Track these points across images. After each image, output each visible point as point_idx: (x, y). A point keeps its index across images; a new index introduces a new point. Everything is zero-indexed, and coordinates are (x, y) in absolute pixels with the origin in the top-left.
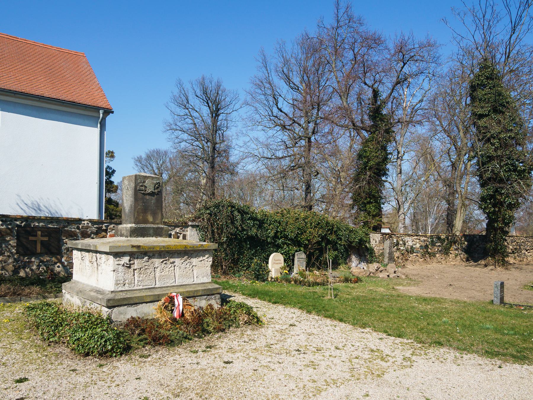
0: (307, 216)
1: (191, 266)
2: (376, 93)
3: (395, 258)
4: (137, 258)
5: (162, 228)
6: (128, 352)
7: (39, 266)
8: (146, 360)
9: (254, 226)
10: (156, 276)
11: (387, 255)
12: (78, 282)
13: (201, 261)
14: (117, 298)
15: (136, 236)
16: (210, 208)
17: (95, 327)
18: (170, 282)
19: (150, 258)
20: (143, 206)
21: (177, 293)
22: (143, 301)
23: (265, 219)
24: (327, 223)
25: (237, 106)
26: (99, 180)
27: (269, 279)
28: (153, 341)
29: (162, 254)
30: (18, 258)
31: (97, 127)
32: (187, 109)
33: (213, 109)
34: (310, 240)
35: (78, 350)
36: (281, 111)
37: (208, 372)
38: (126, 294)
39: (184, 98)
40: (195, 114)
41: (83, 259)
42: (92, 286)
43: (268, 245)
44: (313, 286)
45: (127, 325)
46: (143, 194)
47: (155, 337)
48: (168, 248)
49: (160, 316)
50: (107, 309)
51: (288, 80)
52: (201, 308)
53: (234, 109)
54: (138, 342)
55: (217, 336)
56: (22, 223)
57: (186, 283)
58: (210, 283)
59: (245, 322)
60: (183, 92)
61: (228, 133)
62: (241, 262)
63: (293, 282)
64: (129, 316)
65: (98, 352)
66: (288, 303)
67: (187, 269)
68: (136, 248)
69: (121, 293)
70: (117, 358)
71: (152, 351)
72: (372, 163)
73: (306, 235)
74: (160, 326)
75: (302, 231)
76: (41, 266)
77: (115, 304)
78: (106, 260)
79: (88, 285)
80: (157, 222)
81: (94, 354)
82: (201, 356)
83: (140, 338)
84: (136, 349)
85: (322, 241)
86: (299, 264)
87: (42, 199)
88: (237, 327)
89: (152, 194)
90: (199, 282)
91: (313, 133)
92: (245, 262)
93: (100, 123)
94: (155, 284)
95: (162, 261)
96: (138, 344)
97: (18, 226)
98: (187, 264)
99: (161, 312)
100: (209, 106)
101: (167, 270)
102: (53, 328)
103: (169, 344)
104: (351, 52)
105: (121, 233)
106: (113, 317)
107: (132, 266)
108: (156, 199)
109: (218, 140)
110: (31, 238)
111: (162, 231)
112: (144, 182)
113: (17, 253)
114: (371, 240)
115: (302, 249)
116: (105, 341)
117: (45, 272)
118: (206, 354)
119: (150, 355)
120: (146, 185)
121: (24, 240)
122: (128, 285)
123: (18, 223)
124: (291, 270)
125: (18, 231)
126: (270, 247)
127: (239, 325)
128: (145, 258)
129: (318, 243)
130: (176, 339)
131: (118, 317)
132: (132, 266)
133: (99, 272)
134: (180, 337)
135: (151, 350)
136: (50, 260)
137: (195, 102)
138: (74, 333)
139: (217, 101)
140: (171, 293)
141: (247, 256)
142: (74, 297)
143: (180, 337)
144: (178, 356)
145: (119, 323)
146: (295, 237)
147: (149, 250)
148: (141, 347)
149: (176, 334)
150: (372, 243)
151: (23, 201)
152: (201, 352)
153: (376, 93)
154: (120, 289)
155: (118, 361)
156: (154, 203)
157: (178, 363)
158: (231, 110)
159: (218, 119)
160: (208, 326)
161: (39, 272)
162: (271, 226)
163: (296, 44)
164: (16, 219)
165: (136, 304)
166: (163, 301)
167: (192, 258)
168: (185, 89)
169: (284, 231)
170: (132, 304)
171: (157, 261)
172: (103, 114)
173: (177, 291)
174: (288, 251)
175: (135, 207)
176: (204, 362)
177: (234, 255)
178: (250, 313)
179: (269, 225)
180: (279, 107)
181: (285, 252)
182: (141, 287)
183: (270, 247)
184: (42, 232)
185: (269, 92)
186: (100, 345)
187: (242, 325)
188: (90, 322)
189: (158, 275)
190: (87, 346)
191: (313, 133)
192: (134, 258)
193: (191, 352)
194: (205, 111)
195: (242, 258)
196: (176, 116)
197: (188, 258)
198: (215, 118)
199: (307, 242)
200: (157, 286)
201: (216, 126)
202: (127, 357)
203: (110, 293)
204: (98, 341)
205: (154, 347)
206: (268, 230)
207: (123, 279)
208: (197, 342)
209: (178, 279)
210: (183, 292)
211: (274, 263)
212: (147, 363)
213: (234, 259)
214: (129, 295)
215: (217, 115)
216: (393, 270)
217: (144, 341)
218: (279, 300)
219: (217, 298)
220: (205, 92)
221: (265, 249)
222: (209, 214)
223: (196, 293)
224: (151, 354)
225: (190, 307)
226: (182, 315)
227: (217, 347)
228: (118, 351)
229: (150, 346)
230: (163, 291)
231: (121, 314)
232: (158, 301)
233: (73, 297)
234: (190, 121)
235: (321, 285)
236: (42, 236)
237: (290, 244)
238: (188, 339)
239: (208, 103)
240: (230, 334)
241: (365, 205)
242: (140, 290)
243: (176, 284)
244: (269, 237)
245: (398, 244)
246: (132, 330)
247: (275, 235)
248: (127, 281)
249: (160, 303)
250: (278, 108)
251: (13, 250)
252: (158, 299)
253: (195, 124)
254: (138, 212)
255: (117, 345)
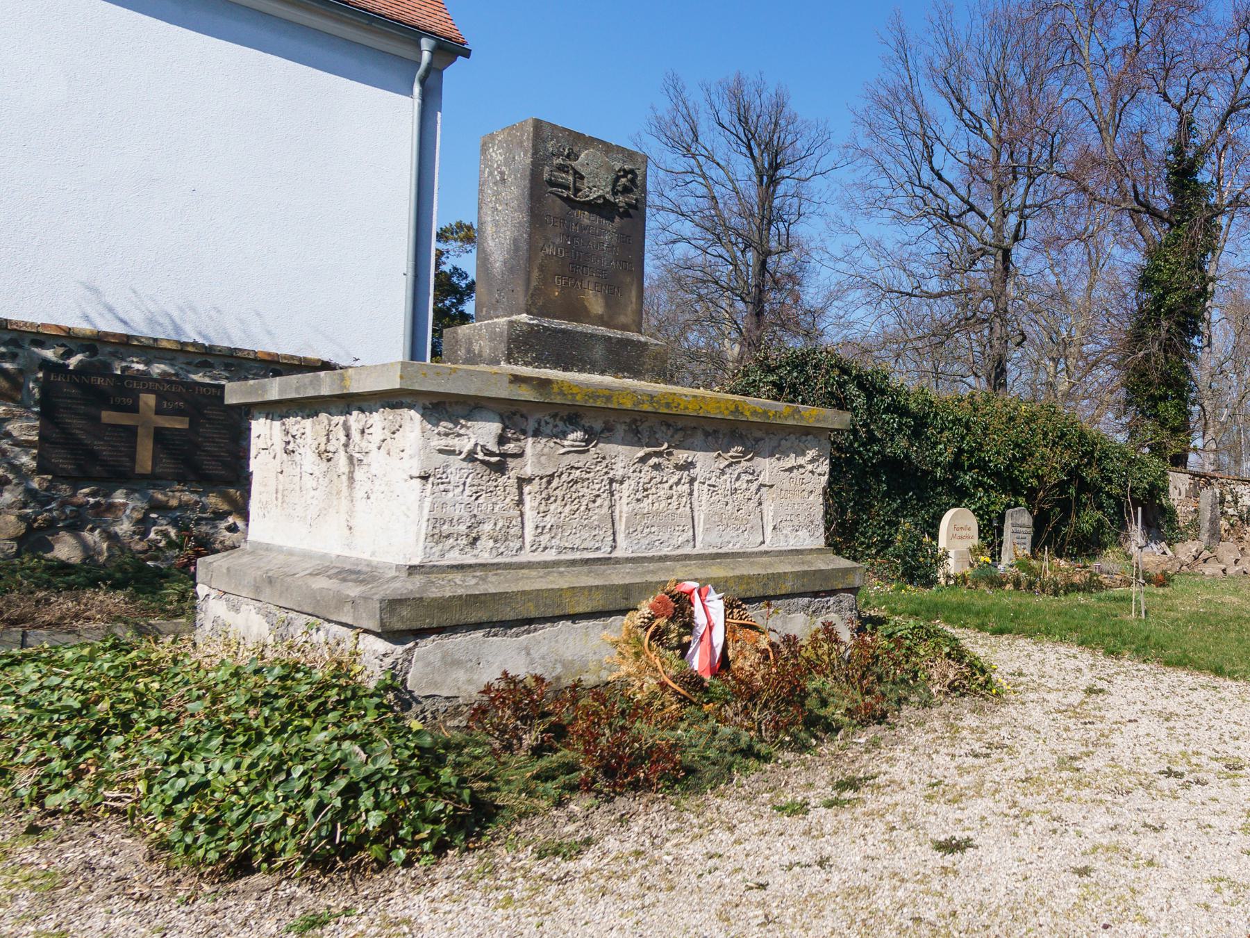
0: (1034, 414)
1: (754, 486)
2: (1186, 125)
3: (1223, 532)
4: (537, 434)
5: (644, 345)
6: (480, 836)
7: (143, 525)
8: (571, 865)
9: (899, 430)
10: (617, 513)
11: (1207, 525)
12: (268, 548)
13: (790, 470)
14: (434, 593)
15: (535, 360)
16: (778, 367)
17: (307, 722)
18: (672, 542)
19: (592, 437)
20: (568, 249)
21: (704, 582)
22: (558, 612)
23: (928, 414)
24: (1082, 436)
25: (825, 164)
26: (411, 264)
27: (942, 581)
28: (605, 774)
29: (644, 427)
30: (47, 489)
31: (410, 93)
32: (694, 156)
33: (763, 165)
34: (1043, 476)
35: (188, 847)
36: (940, 178)
37: (883, 901)
38: (484, 579)
39: (684, 127)
40: (715, 173)
41: (290, 447)
42: (324, 556)
43: (936, 487)
44: (1066, 594)
45: (480, 713)
46: (567, 200)
47: (614, 755)
48: (668, 405)
49: (633, 670)
50: (381, 646)
51: (958, 99)
52: (790, 641)
53: (818, 171)
54: (533, 785)
55: (863, 740)
56: (69, 354)
57: (736, 549)
58: (819, 551)
59: (949, 686)
60: (685, 112)
61: (801, 230)
62: (861, 533)
63: (1009, 587)
64: (491, 675)
65: (306, 850)
66: (1039, 630)
67: (739, 496)
68: (534, 388)
69: (458, 577)
70: (418, 869)
71: (601, 819)
72: (1172, 299)
73: (1035, 464)
74: (636, 711)
75: (1024, 451)
76: (155, 523)
77: (426, 623)
78: (388, 434)
79: (306, 555)
80: (622, 319)
81: (280, 863)
82: (828, 828)
83: (543, 763)
84: (523, 815)
85: (1069, 482)
86: (1016, 541)
87: (193, 309)
88: (926, 705)
89: (603, 208)
90: (783, 546)
91: (1016, 238)
92: (874, 533)
93: (423, 82)
94: (614, 548)
95: (641, 454)
96: (531, 793)
97: (45, 364)
98: (738, 479)
99: (637, 655)
100: (752, 154)
101: (661, 493)
102: (68, 742)
103: (677, 781)
104: (1130, 21)
105: (469, 351)
106: (415, 681)
107: (511, 463)
108: (620, 231)
109: (773, 244)
110: (107, 416)
111: (639, 356)
112: (572, 156)
113: (40, 470)
114: (1171, 489)
115: (1022, 500)
116: (352, 791)
117: (171, 544)
118: (845, 816)
119: (588, 842)
120: (579, 168)
121: (76, 425)
122: (491, 543)
123: (49, 354)
124: (996, 556)
125: (45, 387)
126: (940, 494)
127: (931, 696)
128: (571, 436)
129: (1062, 486)
130: (708, 758)
131: (438, 678)
132: (511, 463)
133: (359, 493)
134: (722, 750)
135: (596, 816)
136: (197, 503)
137: (715, 140)
138: (180, 760)
139: (775, 143)
140: (678, 581)
141: (878, 515)
142: (244, 607)
143: (722, 750)
144: (725, 836)
145: (442, 705)
146: (1007, 468)
147: (591, 403)
148: (544, 804)
149: (703, 741)
150: (1171, 497)
151: (111, 310)
152: (823, 811)
153: (1186, 125)
154: (454, 557)
155: (418, 885)
156: (610, 246)
157: (730, 868)
158: (810, 173)
159: (774, 191)
160: (824, 703)
161: (140, 546)
162: (946, 433)
163: (978, 16)
164: (40, 337)
165: (529, 621)
166: (645, 609)
167: (757, 454)
168: (690, 104)
169: (980, 450)
170: (507, 625)
171: (622, 456)
172: (433, 52)
173: (700, 574)
174: (988, 506)
175: (533, 247)
176: (849, 856)
177: (844, 512)
178: (963, 657)
179: (940, 433)
180: (936, 167)
181: (980, 508)
182: (551, 556)
183: (940, 494)
184: (160, 397)
185: (914, 126)
186: (316, 813)
187: (942, 697)
188: (282, 702)
189: (625, 509)
190: (239, 822)
191: (1016, 238)
192: (524, 432)
193: (780, 809)
194: (743, 168)
195: (867, 521)
196: (661, 173)
197: (745, 453)
198: (768, 187)
199: (1035, 482)
200: (618, 554)
201: (770, 207)
202: (470, 860)
203: (404, 574)
204: (307, 792)
205: (610, 800)
206: (935, 444)
207: (466, 515)
208: (792, 769)
209: (707, 530)
210: (727, 580)
211: (954, 536)
212: (578, 886)
213: (844, 522)
214: (493, 585)
215: (774, 182)
216: (1232, 557)
217: (562, 779)
218: (1010, 625)
219: (845, 604)
220: (743, 120)
221: (928, 499)
222: (774, 383)
223: (772, 584)
224: (595, 834)
225: (753, 633)
226: (723, 664)
227: (881, 780)
228: (424, 835)
229: (588, 800)
230: (644, 573)
231: (457, 663)
232: (623, 612)
233: (237, 611)
234: (701, 190)
235: (1084, 590)
236: (159, 411)
237: (992, 487)
238: (758, 756)
239: (749, 148)
240: (910, 729)
241: (1155, 400)
242: (545, 565)
243: (695, 551)
244: (938, 464)
245: (1222, 501)
246: (503, 732)
247: (955, 459)
248: (487, 527)
249: (634, 619)
250: (932, 169)
251: (25, 459)
252: (622, 605)
253: (714, 198)
254: (542, 269)
255: (419, 807)
